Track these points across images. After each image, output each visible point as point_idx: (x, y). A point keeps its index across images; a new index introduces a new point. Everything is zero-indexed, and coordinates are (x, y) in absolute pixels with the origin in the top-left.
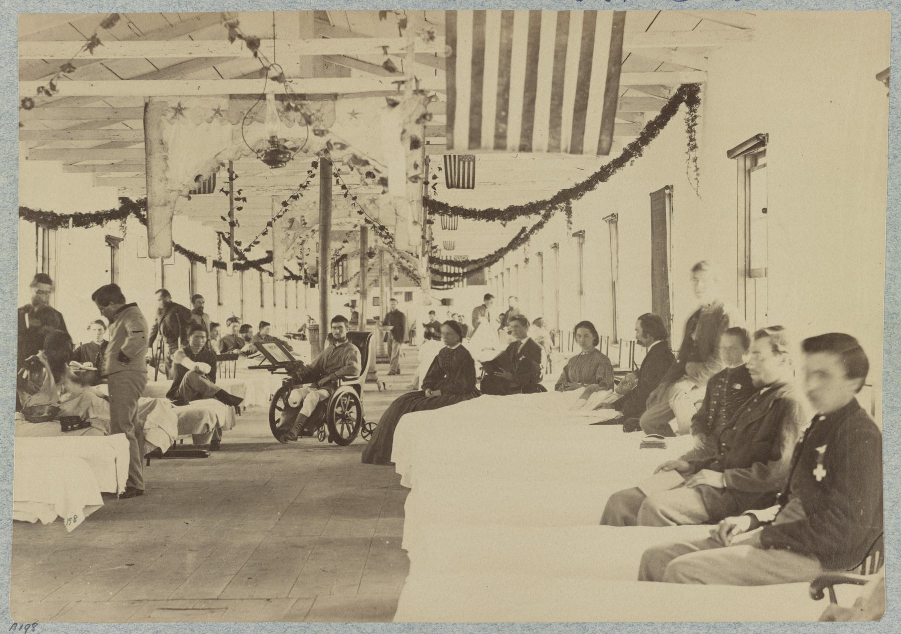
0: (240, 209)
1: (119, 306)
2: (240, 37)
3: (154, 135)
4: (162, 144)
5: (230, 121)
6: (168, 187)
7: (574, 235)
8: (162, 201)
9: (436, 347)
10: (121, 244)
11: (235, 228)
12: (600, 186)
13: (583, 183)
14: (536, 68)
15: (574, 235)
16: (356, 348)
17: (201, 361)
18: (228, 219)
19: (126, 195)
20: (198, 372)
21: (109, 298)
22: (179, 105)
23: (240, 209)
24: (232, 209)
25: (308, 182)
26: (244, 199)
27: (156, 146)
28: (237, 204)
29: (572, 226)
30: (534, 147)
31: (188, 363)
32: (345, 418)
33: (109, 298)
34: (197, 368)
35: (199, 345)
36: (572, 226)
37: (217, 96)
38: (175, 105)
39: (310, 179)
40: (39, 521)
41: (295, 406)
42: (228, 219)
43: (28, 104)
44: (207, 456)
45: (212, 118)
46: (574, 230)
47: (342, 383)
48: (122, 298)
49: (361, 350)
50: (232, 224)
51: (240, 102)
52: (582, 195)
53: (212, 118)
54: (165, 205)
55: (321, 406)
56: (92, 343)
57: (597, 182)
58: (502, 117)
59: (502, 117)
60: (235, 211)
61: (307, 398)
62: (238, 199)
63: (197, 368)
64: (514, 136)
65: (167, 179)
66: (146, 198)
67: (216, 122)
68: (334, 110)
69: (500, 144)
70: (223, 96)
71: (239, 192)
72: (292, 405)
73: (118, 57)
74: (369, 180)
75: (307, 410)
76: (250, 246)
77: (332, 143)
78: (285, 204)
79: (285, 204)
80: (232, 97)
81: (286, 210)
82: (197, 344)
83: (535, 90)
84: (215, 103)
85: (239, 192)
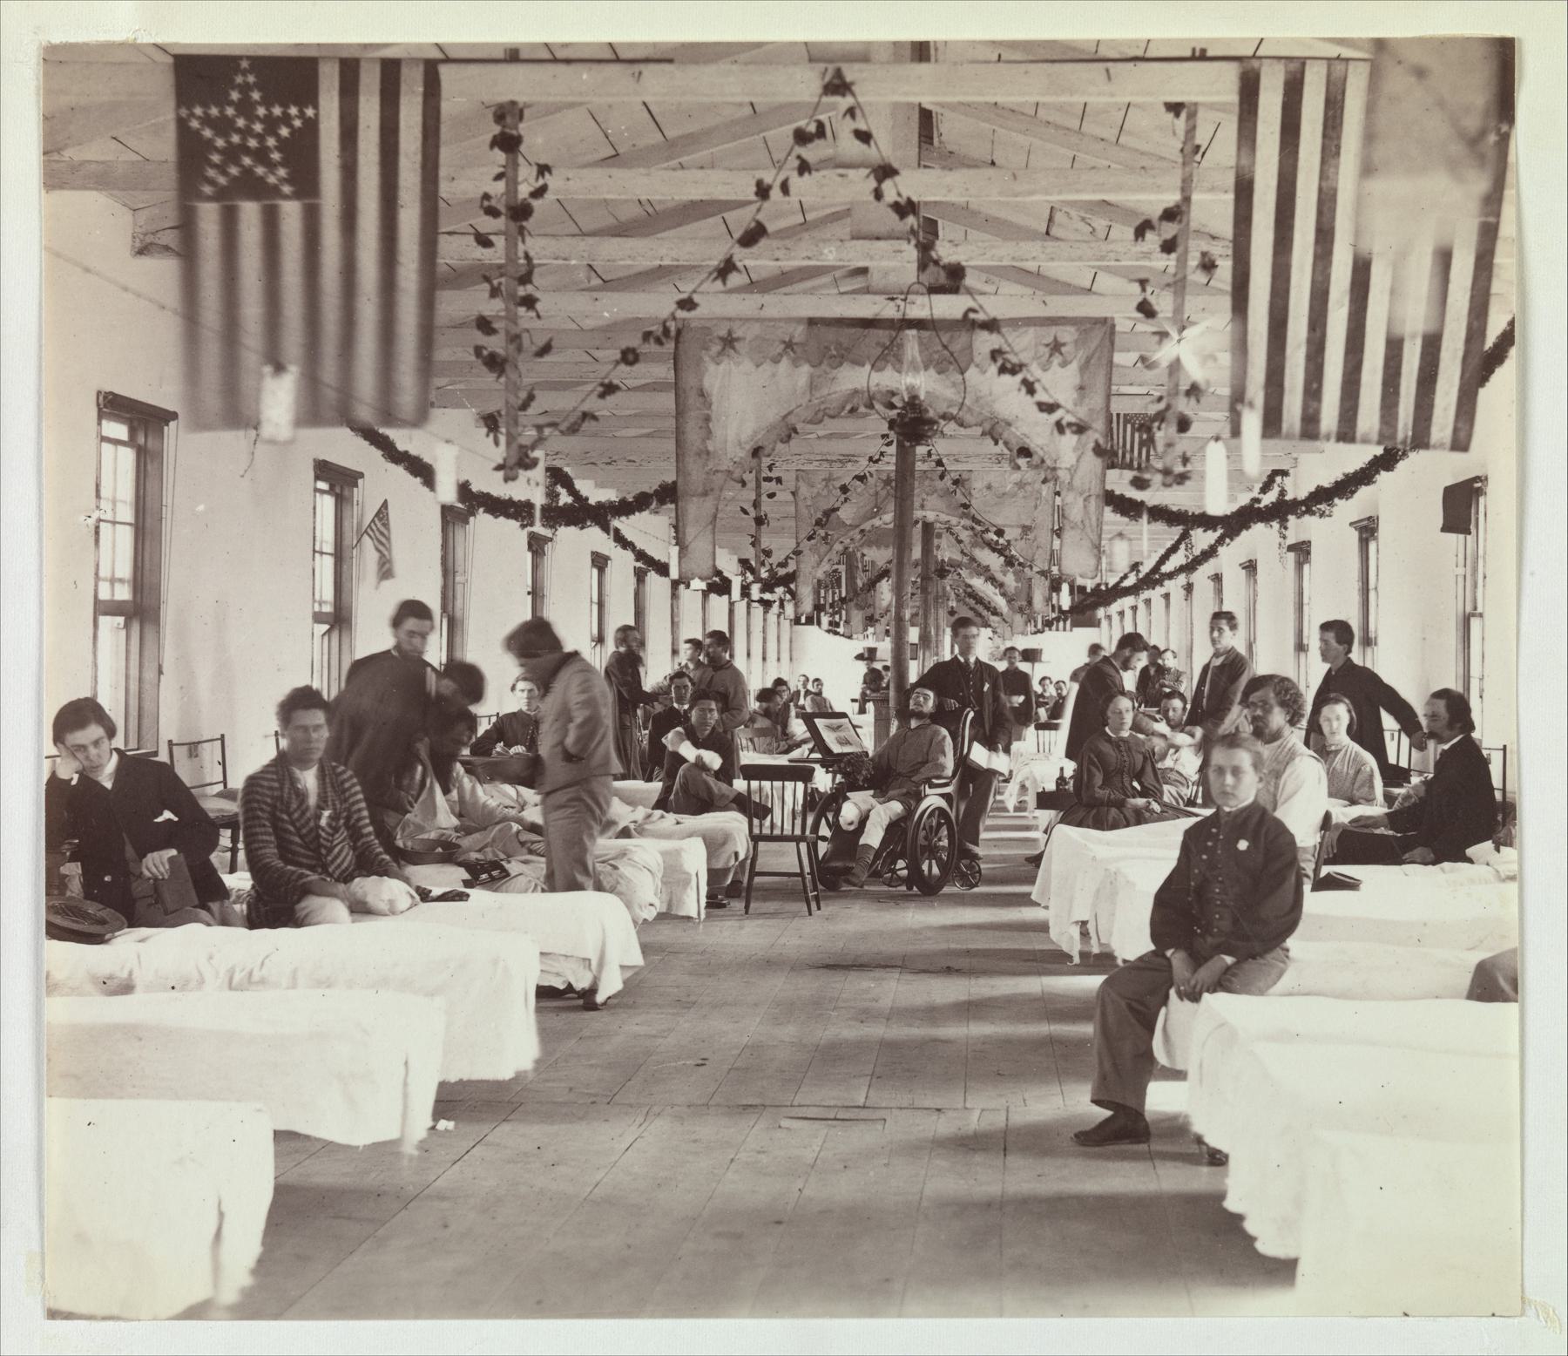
0: (771, 496)
1: (556, 656)
2: (936, 263)
3: (690, 380)
4: (702, 395)
5: (809, 361)
6: (711, 465)
7: (1291, 548)
8: (700, 490)
9: (1227, 726)
10: (548, 547)
11: (764, 527)
12: (1383, 477)
13: (1356, 473)
14: (1364, 318)
15: (1291, 548)
16: (944, 732)
17: (707, 748)
18: (753, 513)
19: (558, 463)
20: (700, 765)
21: (536, 644)
22: (730, 333)
23: (771, 496)
24: (759, 495)
25: (882, 454)
26: (779, 480)
27: (692, 400)
28: (767, 487)
29: (1287, 533)
30: (1358, 435)
31: (688, 751)
32: (932, 851)
33: (536, 644)
34: (699, 758)
35: (706, 724)
36: (1287, 533)
37: (789, 320)
38: (723, 333)
39: (884, 449)
40: (570, 985)
41: (852, 828)
42: (753, 513)
43: (631, 357)
44: (724, 906)
45: (781, 355)
46: (1291, 540)
47: (928, 791)
48: (556, 643)
49: (954, 739)
50: (760, 521)
51: (823, 329)
52: (1353, 492)
53: (781, 355)
54: (705, 494)
55: (895, 829)
56: (521, 711)
57: (1378, 472)
58: (1313, 390)
59: (1313, 390)
60: (764, 498)
61: (872, 815)
62: (768, 479)
63: (699, 758)
64: (1329, 417)
65: (708, 453)
66: (674, 483)
67: (785, 363)
68: (970, 346)
69: (1310, 428)
70: (799, 320)
71: (770, 468)
72: (845, 827)
73: (666, 262)
74: (1022, 462)
75: (873, 837)
76: (788, 557)
77: (1064, 422)
78: (844, 489)
79: (844, 489)
80: (812, 322)
81: (846, 500)
82: (703, 721)
83: (1362, 351)
84: (783, 332)
85: (770, 468)
